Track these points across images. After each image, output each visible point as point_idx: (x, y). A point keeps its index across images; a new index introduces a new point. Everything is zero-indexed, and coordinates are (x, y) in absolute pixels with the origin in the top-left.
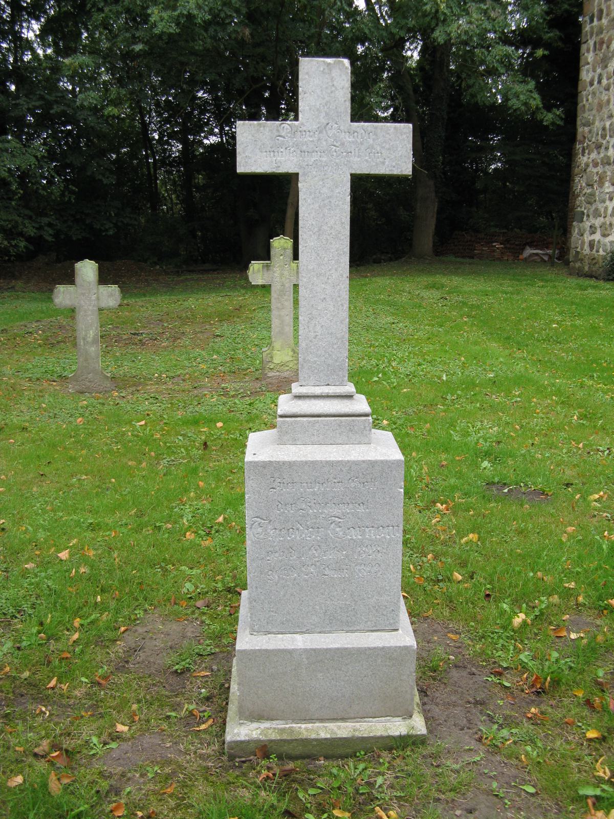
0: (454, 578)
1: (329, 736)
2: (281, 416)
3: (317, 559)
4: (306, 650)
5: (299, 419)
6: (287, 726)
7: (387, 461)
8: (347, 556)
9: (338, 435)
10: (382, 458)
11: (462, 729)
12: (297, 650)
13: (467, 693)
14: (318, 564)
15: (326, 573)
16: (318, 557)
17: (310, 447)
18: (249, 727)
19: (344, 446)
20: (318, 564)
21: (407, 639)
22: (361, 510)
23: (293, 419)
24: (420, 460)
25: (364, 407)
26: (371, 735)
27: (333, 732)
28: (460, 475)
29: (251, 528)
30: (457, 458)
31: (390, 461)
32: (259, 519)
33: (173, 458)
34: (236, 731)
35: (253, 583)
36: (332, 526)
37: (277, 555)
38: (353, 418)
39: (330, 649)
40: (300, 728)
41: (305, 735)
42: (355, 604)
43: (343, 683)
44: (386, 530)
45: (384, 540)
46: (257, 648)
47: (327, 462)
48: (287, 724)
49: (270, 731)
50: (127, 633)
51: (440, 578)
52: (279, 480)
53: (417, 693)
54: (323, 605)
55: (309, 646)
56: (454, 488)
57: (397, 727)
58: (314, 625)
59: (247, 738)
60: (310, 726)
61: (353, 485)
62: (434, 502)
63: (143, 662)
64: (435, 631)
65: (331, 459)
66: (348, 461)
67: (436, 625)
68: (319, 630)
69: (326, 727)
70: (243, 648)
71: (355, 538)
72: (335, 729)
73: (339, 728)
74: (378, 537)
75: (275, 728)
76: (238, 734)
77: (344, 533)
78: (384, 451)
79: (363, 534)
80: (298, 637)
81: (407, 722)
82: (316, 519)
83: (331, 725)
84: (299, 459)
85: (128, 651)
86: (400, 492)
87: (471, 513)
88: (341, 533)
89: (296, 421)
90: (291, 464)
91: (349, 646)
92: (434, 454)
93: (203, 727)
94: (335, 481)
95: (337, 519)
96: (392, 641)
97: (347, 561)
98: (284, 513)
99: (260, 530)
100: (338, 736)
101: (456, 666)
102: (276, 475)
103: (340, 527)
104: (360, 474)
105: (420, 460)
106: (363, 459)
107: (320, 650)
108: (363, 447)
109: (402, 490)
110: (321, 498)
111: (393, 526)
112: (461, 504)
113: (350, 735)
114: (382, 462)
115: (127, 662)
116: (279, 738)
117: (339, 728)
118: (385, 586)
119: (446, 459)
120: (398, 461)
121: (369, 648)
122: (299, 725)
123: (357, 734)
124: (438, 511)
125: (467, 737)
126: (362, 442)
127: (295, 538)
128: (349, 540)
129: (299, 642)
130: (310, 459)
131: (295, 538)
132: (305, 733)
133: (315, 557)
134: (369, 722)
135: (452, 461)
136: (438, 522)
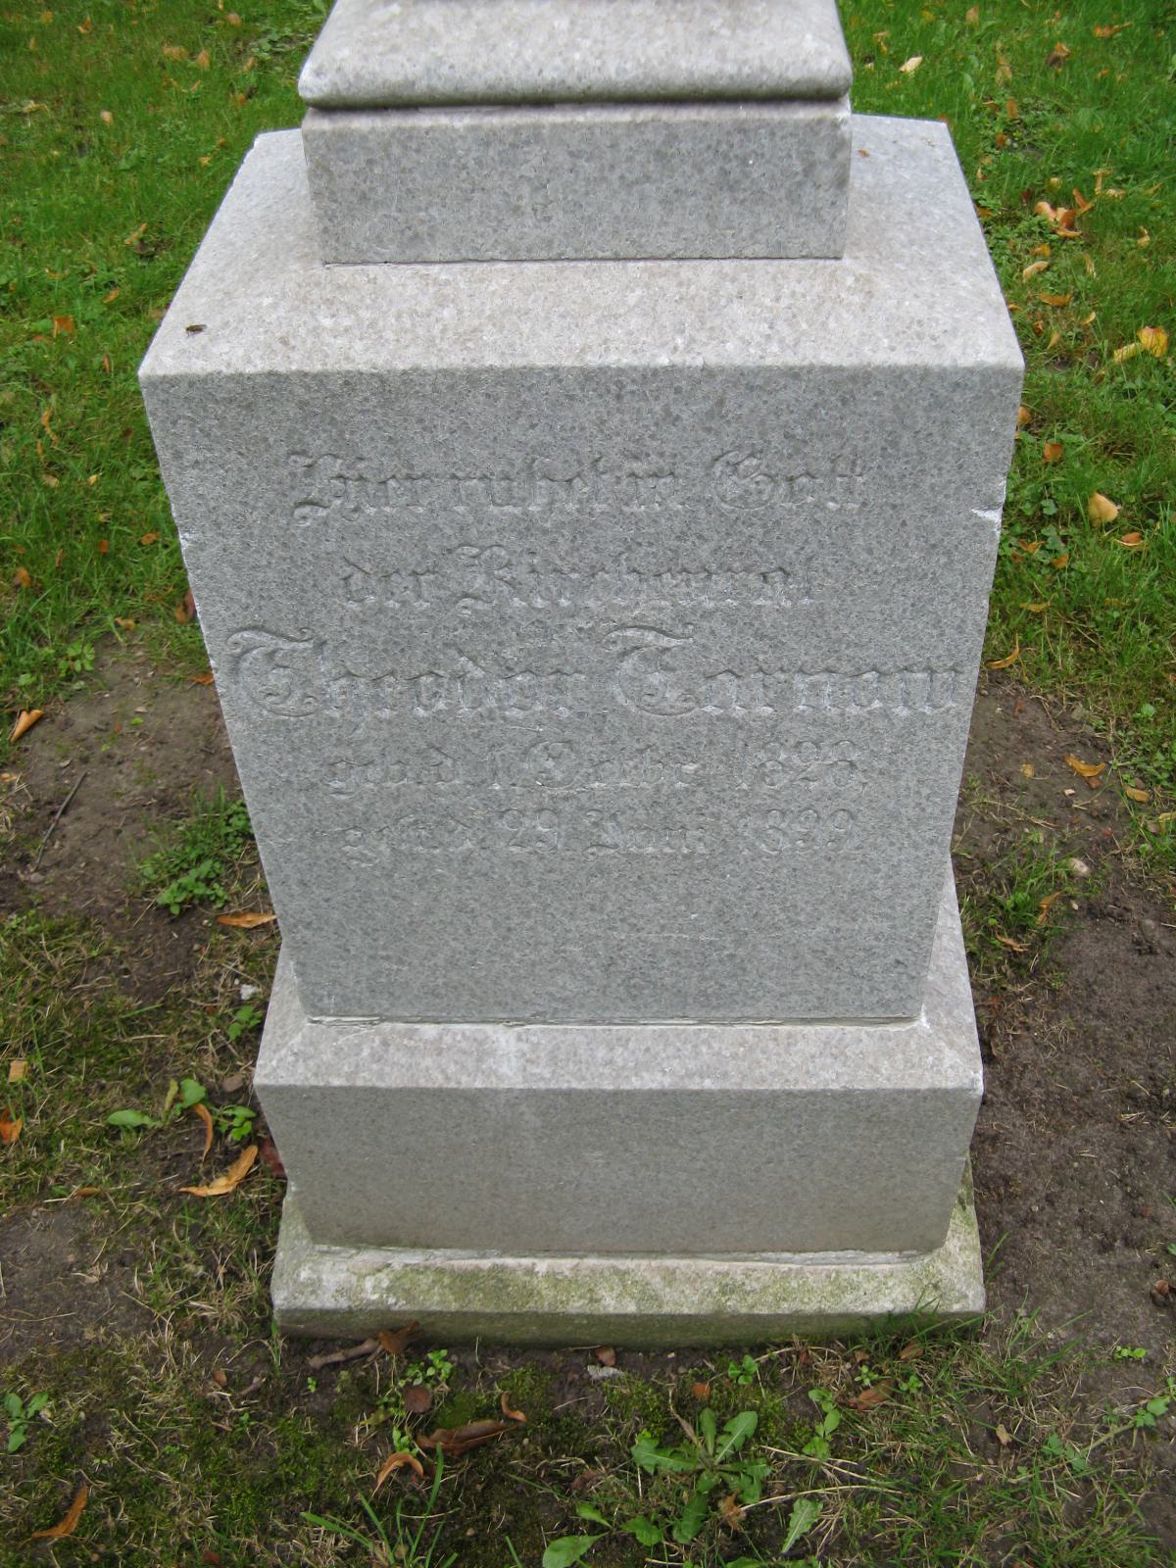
0: (1093, 510)
1: (631, 1308)
2: (328, 107)
3: (560, 791)
4: (530, 1095)
5: (424, 121)
6: (486, 1264)
7: (926, 372)
8: (700, 781)
9: (654, 210)
10: (901, 358)
11: (1105, 1248)
12: (496, 1092)
13: (1125, 1045)
14: (567, 808)
15: (606, 839)
16: (567, 782)
17: (499, 278)
18: (350, 1263)
19: (686, 270)
20: (567, 808)
21: (950, 1057)
22: (772, 600)
23: (394, 122)
24: (992, 34)
25: (810, 43)
26: (785, 1308)
27: (647, 1294)
28: (1106, 97)
29: (235, 671)
30: (1099, 32)
31: (942, 374)
32: (265, 638)
33: (288, 31)
34: (304, 1274)
35: (288, 869)
36: (627, 665)
37: (373, 773)
38: (743, 113)
39: (631, 1094)
40: (530, 1271)
41: (547, 1300)
42: (738, 943)
43: (684, 1176)
44: (895, 684)
45: (880, 724)
46: (336, 1082)
47: (589, 377)
48: (483, 1257)
49: (425, 1281)
50: (40, 731)
51: (1050, 509)
52: (338, 466)
53: (950, 872)
54: (599, 945)
55: (544, 1077)
56: (1090, 147)
57: (881, 1285)
58: (564, 1000)
59: (344, 1303)
60: (565, 1265)
61: (731, 487)
62: (1030, 197)
63: (72, 860)
64: (1028, 740)
65: (612, 359)
66: (708, 373)
67: (1032, 711)
68: (586, 1017)
69: (622, 1274)
70: (284, 1079)
71: (738, 712)
72: (657, 1282)
73: (670, 1277)
74: (853, 710)
75: (441, 1271)
76: (315, 1285)
77: (689, 693)
78: (913, 307)
79: (782, 698)
80: (503, 1038)
81: (917, 1265)
82: (547, 635)
83: (640, 1267)
84: (432, 362)
85: (31, 817)
86: (984, 525)
87: (1145, 240)
88: (672, 695)
89: (410, 134)
90: (390, 390)
91: (708, 1084)
92: (1032, 16)
93: (221, 1186)
94: (637, 467)
95: (650, 637)
96: (885, 1066)
97: (701, 796)
98: (382, 610)
99: (277, 679)
100: (666, 1309)
101: (1093, 912)
102: (316, 443)
103: (666, 668)
104: (776, 438)
105: (992, 34)
106: (792, 360)
107: (587, 1096)
108: (797, 279)
109: (995, 516)
110: (564, 546)
111: (931, 671)
112: (1114, 205)
113: (707, 1308)
114: (897, 376)
115: (24, 860)
116: (454, 1307)
117: (670, 1277)
118: (873, 886)
119: (1066, 36)
120: (990, 377)
121: (790, 1094)
122: (526, 1262)
123: (734, 1304)
124: (1044, 231)
125: (1121, 1292)
126: (794, 247)
127: (452, 710)
128: (712, 721)
129: (508, 1057)
130: (492, 360)
131: (452, 710)
132: (548, 1294)
133: (549, 782)
134: (778, 1261)
135: (1083, 42)
136: (1040, 273)
